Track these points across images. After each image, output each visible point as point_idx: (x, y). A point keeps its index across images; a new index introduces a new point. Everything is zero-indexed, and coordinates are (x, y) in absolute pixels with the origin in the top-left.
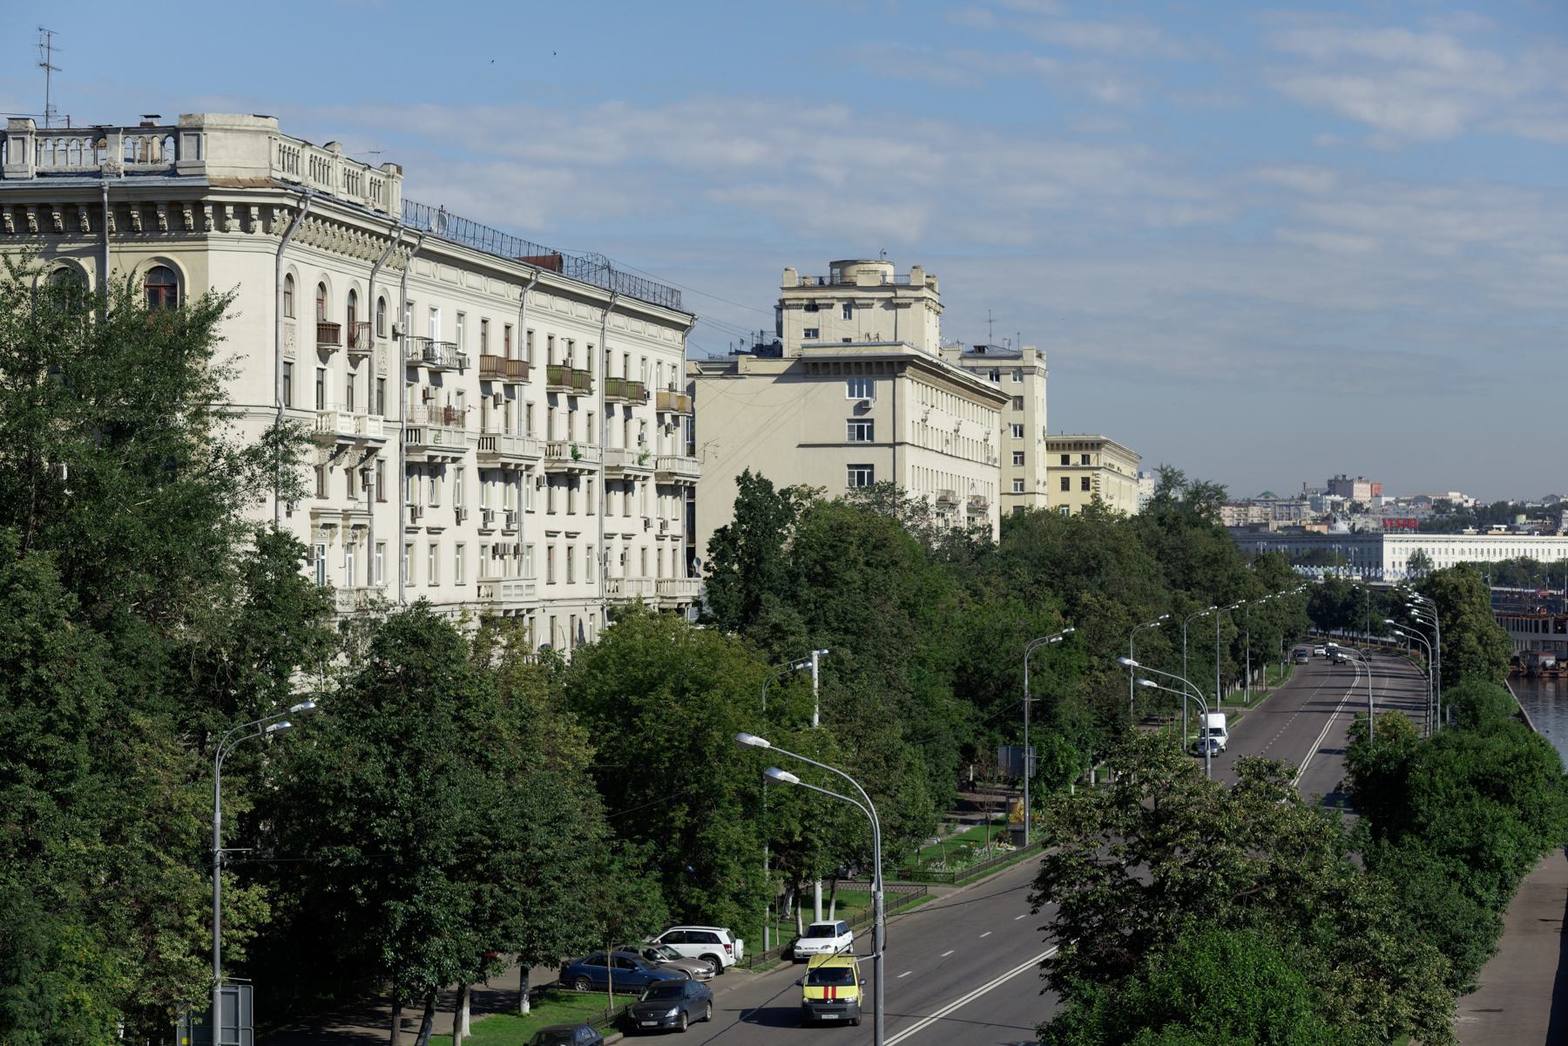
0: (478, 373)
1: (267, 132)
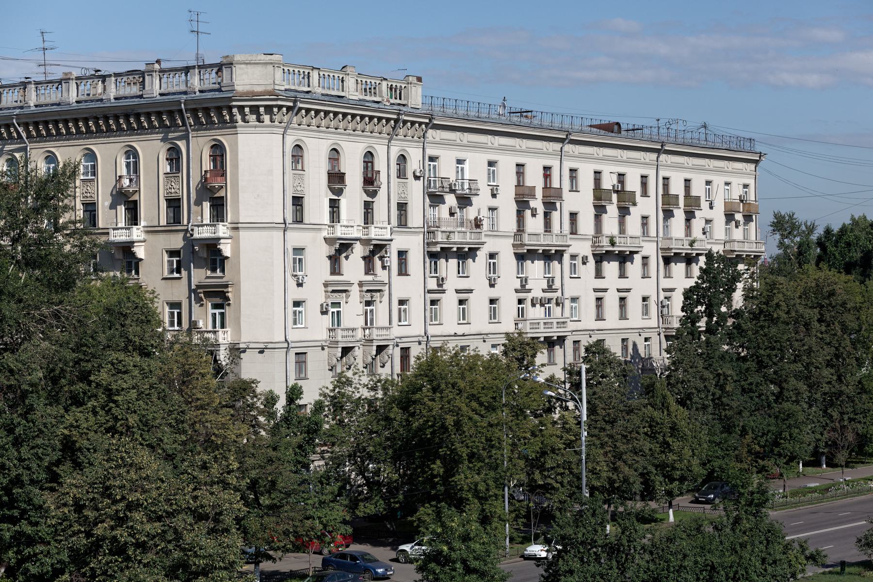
1: (272, 63)
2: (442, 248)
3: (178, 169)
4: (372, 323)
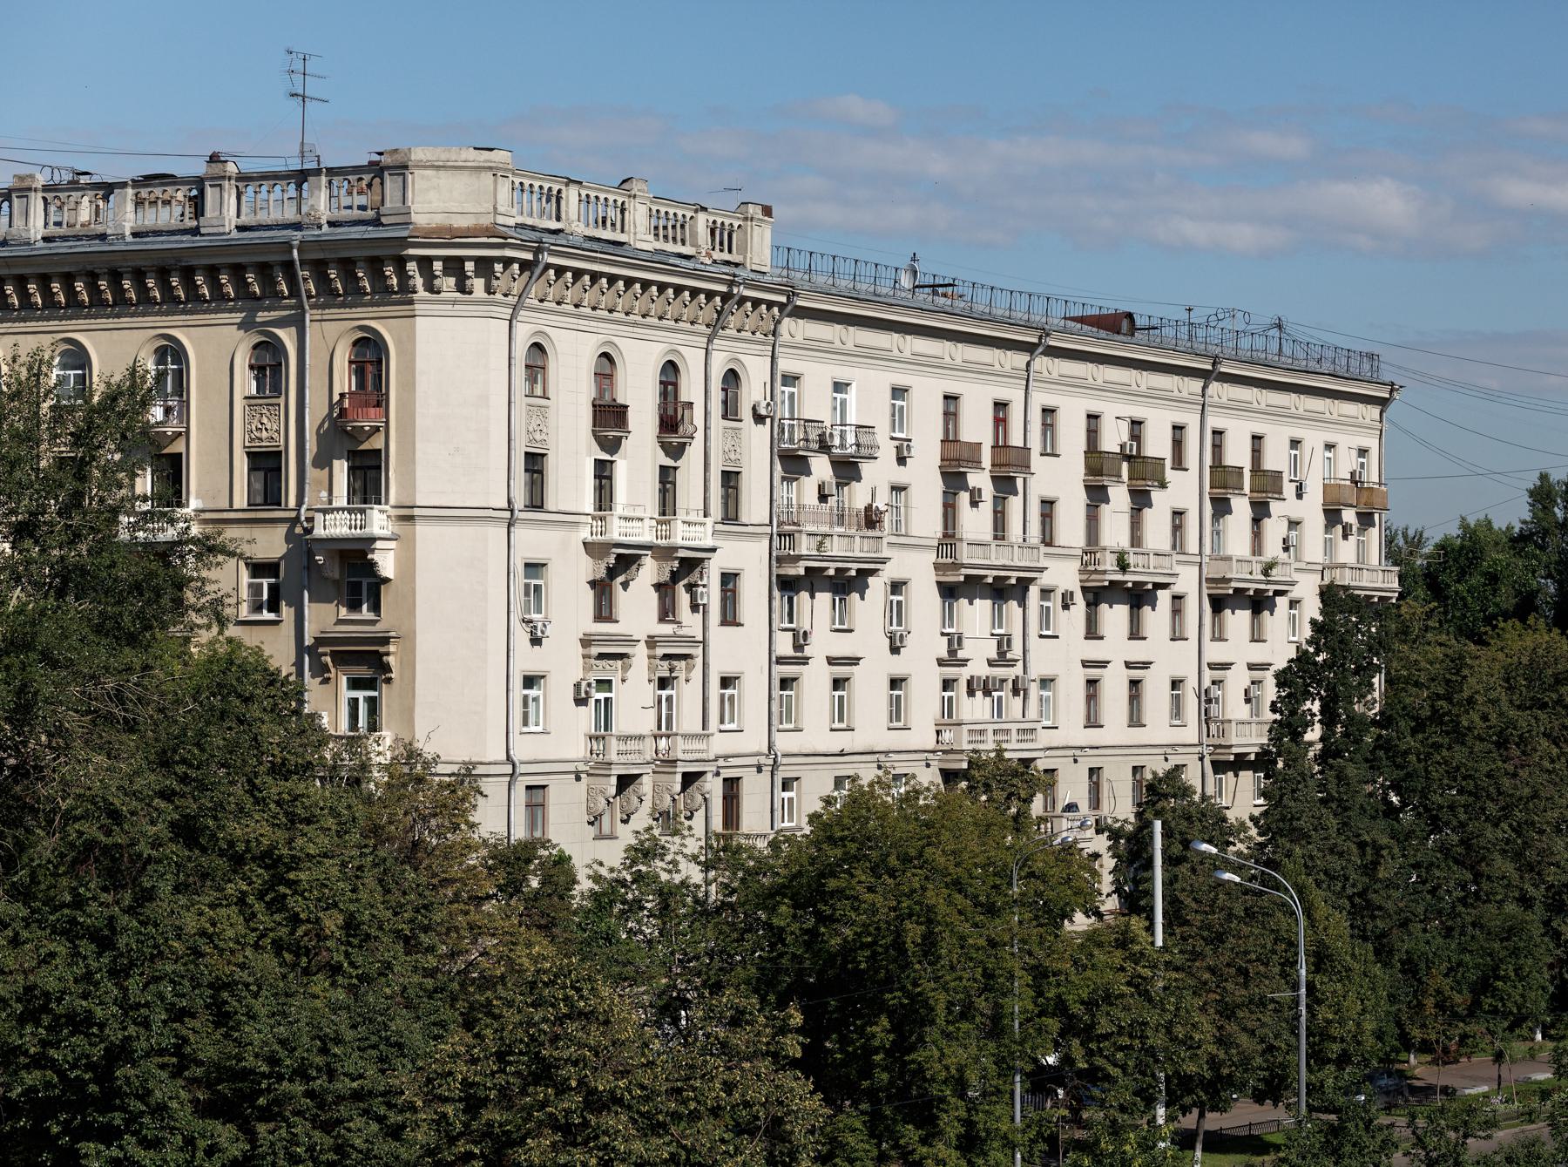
0: (939, 463)
1: (490, 168)
2: (807, 569)
3: (278, 389)
4: (669, 726)
